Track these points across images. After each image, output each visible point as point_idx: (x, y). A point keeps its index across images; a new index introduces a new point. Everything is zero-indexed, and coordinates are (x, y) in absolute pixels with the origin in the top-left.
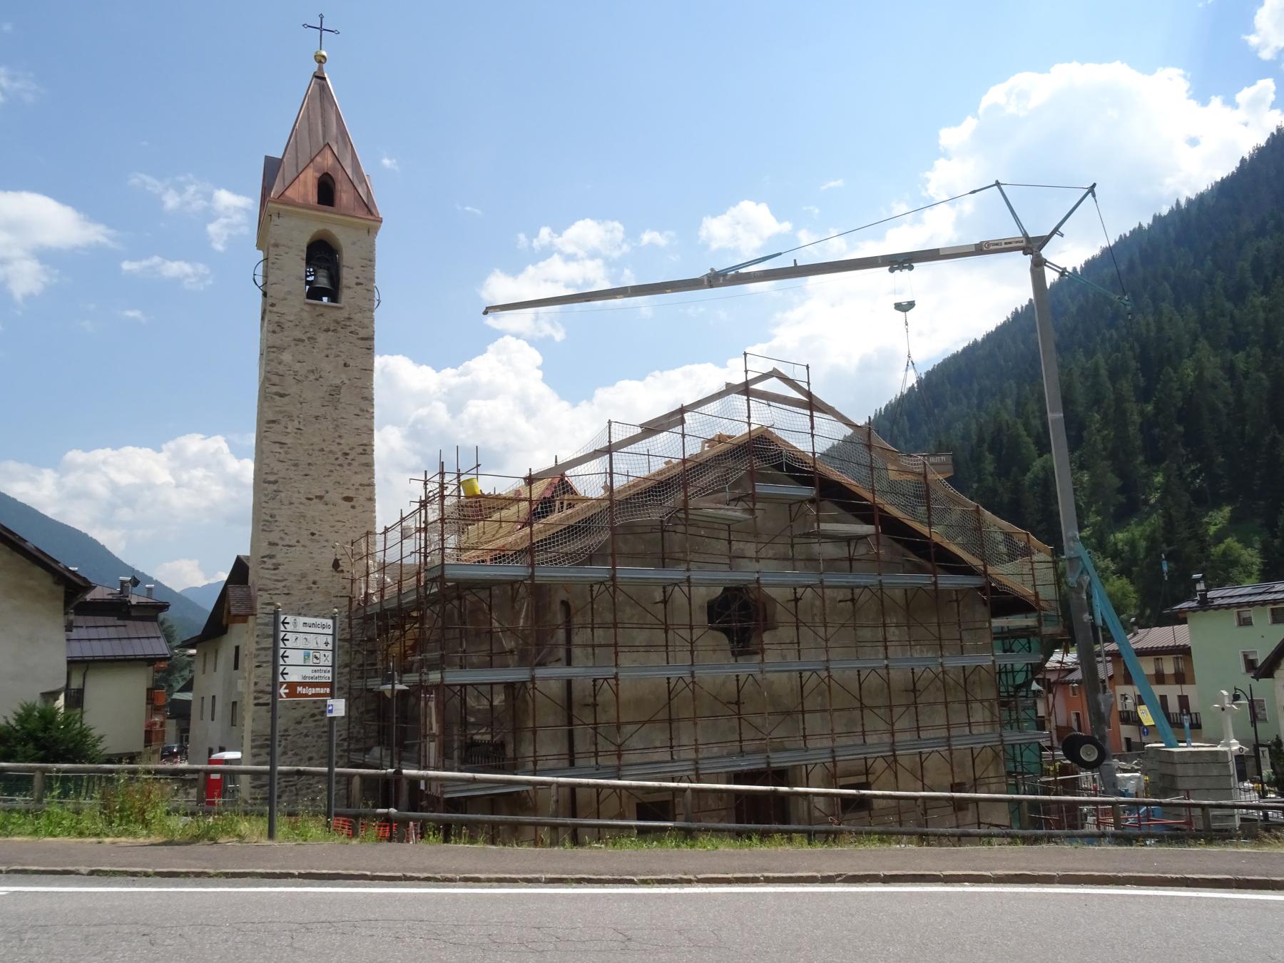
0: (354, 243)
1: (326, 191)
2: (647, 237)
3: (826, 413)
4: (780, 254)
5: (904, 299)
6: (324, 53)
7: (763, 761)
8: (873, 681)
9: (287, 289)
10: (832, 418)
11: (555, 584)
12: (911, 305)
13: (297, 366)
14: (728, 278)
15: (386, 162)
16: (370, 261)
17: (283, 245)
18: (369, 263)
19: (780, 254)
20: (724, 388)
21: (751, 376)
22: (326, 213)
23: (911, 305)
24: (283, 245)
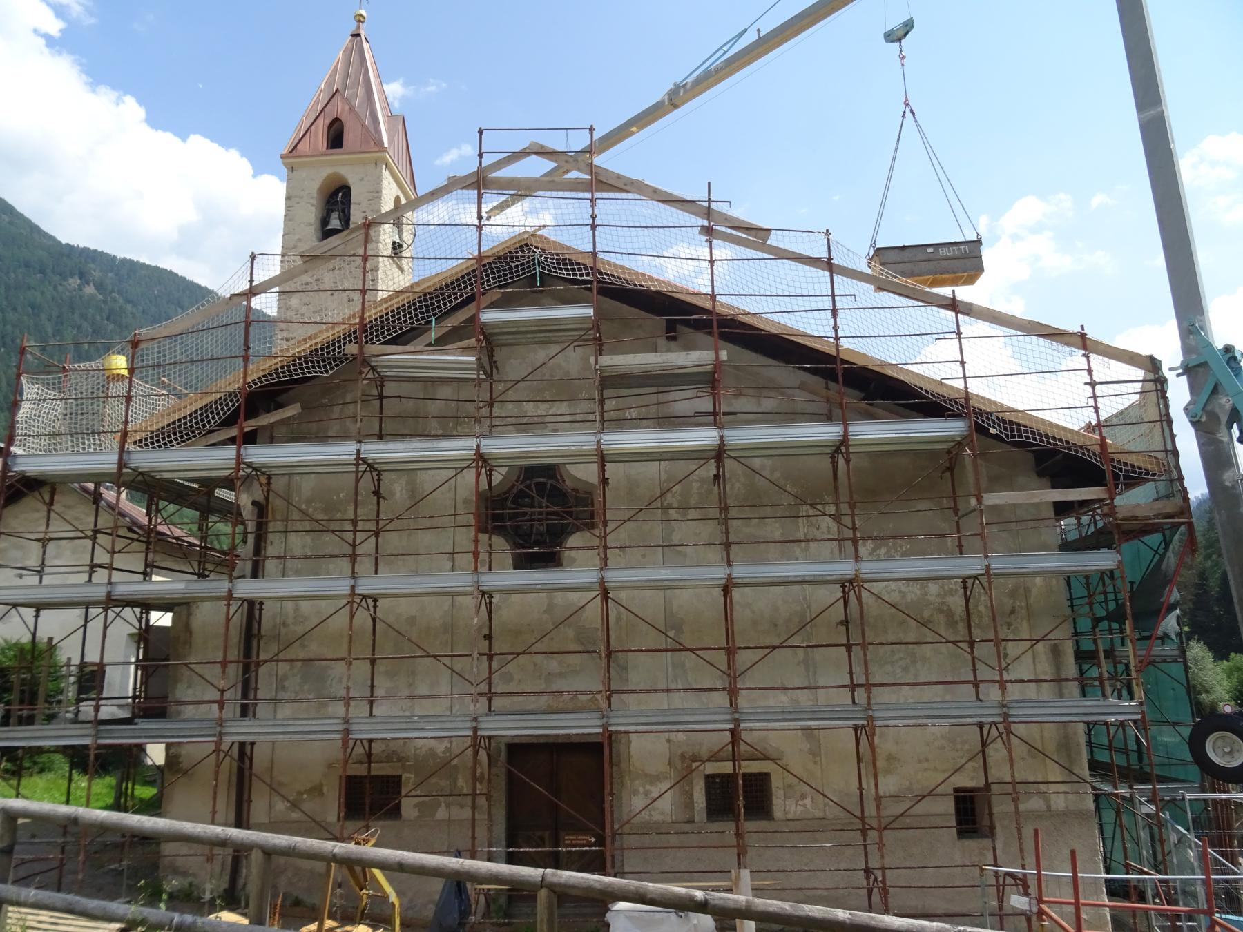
0: (362, 179)
1: (336, 138)
2: (1097, 200)
3: (627, 191)
4: (745, 31)
5: (895, 22)
6: (363, 12)
7: (469, 725)
8: (365, 565)
9: (297, 237)
10: (638, 197)
11: (776, 560)
12: (908, 26)
13: (304, 309)
14: (688, 87)
15: (836, 198)
16: (378, 192)
17: (296, 197)
18: (376, 195)
19: (745, 31)
20: (446, 183)
21: (488, 160)
22: (337, 156)
23: (908, 26)
24: (296, 197)
